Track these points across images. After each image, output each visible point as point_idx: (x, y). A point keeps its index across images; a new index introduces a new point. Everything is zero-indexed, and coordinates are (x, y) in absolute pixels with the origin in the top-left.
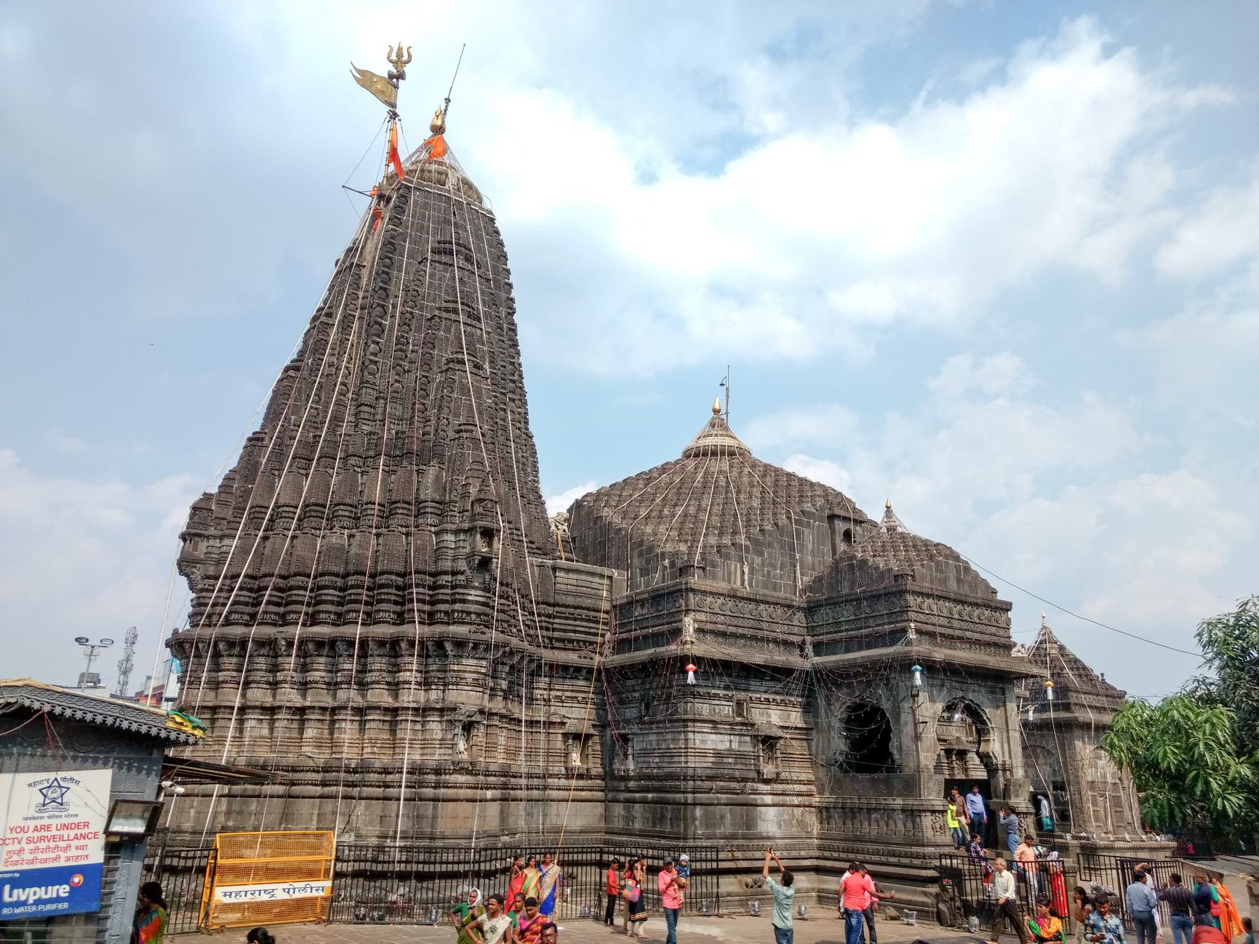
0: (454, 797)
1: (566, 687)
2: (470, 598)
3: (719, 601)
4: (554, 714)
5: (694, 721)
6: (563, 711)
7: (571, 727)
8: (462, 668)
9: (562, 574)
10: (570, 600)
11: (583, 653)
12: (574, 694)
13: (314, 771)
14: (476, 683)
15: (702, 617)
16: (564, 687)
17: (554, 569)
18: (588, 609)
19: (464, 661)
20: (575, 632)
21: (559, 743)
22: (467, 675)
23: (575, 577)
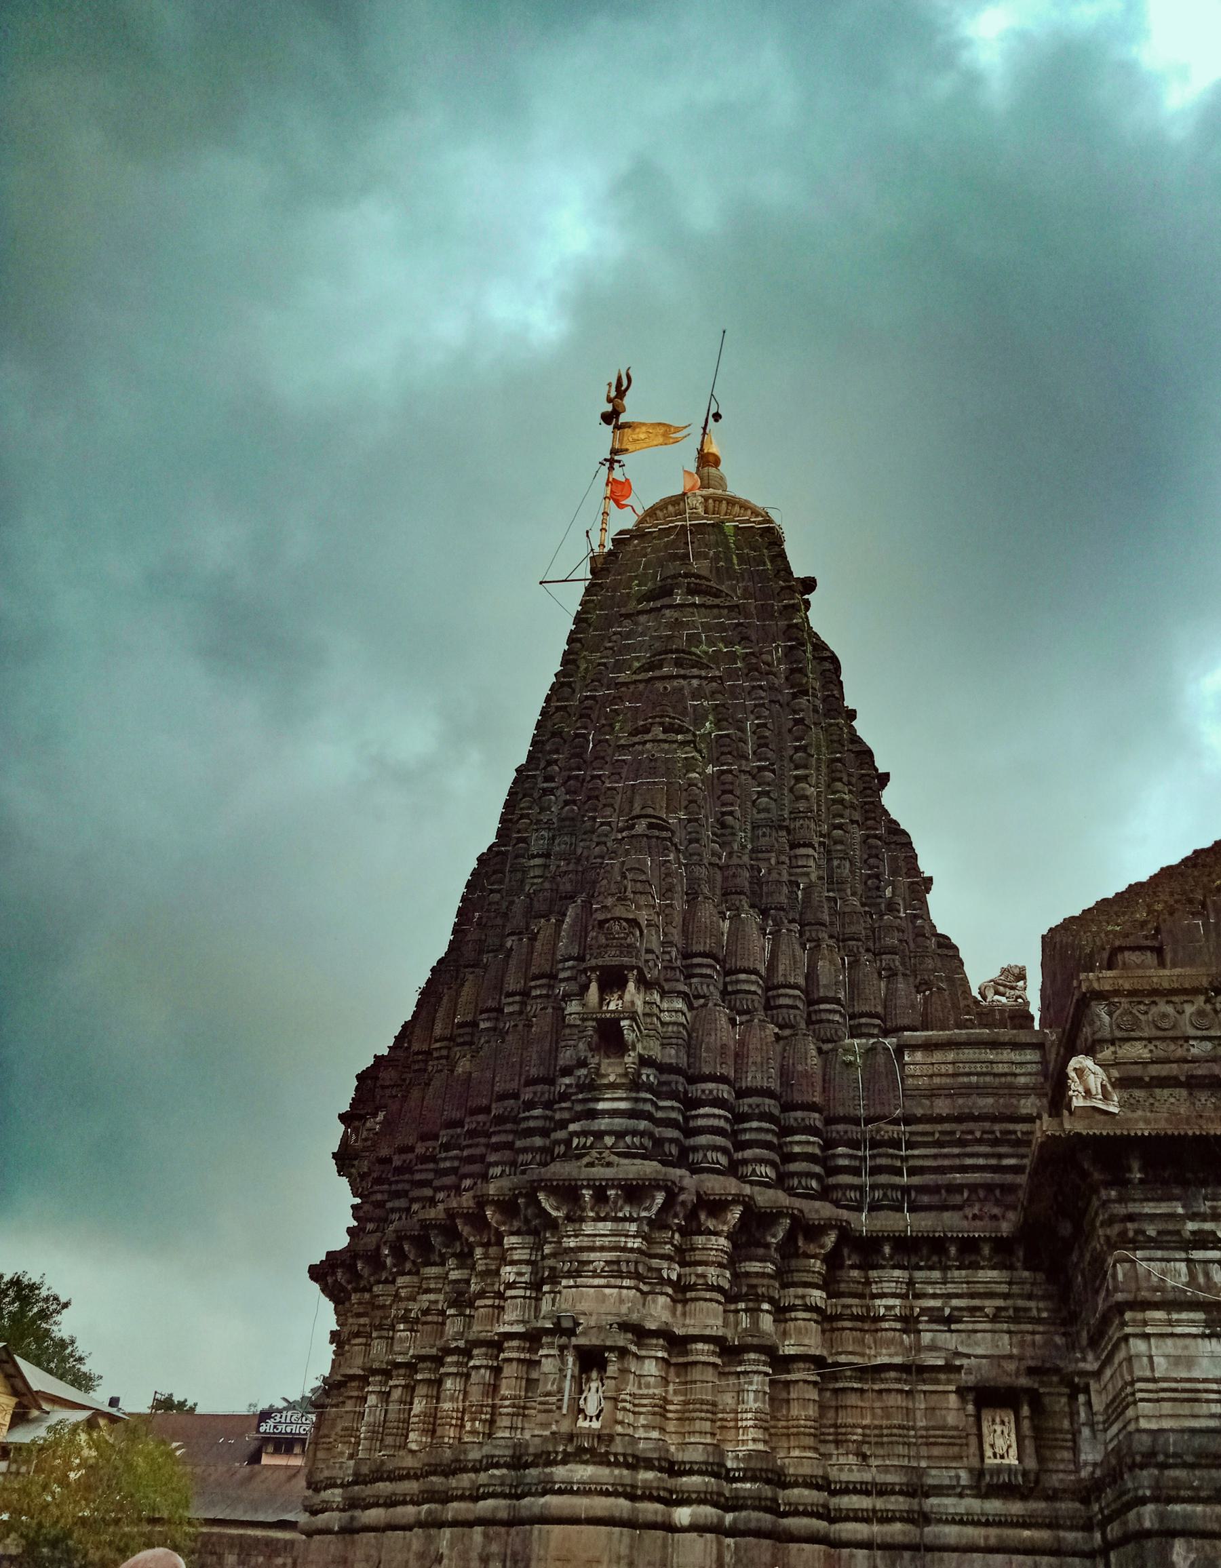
0: (566, 1513)
1: (951, 1288)
2: (601, 1106)
3: (1189, 1009)
4: (933, 1348)
5: (798, 1271)
6: (950, 1341)
7: (975, 1370)
8: (586, 1242)
9: (919, 1056)
10: (942, 1107)
11: (969, 1212)
12: (976, 1302)
13: (807, 1485)
14: (615, 1271)
15: (1138, 1051)
16: (938, 1286)
17: (900, 1050)
18: (994, 1119)
19: (588, 1228)
20: (964, 1169)
21: (953, 1411)
22: (592, 1256)
23: (951, 1056)
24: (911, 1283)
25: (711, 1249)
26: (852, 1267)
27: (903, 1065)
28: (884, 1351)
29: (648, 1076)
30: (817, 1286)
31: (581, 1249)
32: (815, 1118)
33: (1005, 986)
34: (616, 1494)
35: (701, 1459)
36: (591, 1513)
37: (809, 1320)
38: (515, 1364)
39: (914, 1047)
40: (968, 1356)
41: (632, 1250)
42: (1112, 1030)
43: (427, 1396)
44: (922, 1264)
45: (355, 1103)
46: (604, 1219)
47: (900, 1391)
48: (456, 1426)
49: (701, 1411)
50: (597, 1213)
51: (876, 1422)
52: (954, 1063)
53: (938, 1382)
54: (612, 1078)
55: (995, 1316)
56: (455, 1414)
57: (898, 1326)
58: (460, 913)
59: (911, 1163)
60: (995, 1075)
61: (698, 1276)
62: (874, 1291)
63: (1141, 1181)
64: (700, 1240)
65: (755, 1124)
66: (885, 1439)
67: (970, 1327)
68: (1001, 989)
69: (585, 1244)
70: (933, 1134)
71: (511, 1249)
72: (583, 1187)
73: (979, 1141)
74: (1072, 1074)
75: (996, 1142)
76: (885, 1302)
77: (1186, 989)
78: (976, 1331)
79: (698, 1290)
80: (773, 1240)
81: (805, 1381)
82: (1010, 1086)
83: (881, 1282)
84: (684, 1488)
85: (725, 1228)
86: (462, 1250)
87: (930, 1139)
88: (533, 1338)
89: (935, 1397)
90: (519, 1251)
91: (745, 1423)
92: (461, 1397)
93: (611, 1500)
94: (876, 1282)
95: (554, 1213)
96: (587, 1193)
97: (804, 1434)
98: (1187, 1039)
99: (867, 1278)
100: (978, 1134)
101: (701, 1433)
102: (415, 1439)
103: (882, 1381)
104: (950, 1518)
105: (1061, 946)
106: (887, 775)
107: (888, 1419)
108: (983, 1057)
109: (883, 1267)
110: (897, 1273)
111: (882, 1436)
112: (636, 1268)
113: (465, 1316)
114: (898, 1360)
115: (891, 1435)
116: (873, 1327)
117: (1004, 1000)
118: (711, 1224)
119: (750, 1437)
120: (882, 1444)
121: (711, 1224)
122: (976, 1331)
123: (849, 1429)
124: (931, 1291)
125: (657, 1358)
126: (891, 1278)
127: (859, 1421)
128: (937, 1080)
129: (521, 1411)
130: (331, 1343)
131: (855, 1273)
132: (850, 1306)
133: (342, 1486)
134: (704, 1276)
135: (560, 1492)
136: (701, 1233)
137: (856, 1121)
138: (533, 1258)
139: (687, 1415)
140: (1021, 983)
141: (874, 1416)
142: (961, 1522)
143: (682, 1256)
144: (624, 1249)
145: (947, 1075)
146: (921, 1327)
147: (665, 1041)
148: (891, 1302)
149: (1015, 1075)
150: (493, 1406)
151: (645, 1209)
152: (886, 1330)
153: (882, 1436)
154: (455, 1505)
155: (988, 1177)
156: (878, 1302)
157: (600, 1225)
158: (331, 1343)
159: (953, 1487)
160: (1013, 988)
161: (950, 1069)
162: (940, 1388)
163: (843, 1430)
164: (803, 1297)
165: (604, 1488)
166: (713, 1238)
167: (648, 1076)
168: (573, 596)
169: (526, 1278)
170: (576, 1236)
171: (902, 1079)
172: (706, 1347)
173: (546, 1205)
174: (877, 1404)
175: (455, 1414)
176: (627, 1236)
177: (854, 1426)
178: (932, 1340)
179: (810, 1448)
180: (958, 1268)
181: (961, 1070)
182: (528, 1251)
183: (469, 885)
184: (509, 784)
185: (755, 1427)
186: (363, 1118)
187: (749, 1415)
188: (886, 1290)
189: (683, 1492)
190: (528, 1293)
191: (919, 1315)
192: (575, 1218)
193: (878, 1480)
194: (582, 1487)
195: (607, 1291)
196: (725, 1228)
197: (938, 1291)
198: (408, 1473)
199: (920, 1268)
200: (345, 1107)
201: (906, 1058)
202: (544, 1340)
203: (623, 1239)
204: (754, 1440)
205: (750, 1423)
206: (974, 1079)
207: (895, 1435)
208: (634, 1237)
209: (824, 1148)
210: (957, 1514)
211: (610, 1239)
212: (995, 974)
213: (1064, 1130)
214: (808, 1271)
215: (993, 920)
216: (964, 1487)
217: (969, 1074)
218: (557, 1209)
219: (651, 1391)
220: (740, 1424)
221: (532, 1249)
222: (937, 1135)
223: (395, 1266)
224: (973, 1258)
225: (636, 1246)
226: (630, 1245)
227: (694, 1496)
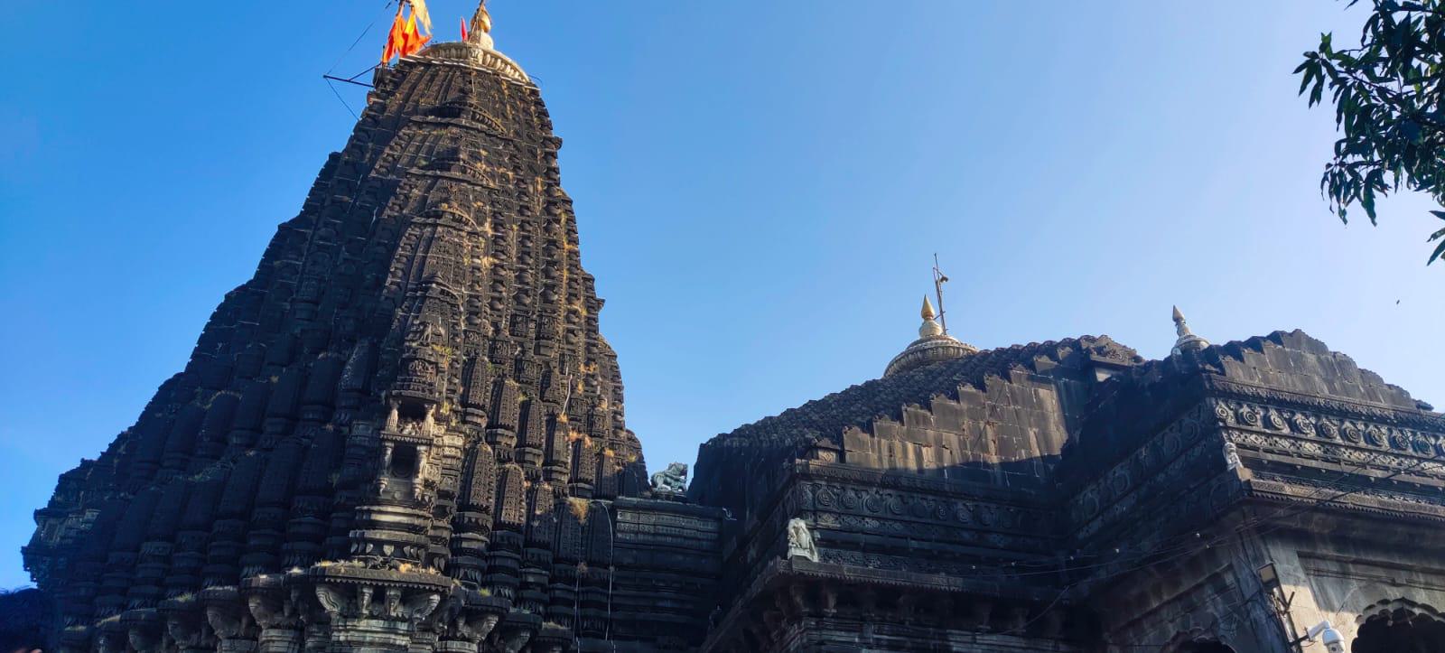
9: (628, 516)
19: (363, 624)
27: (615, 522)
32: (547, 555)
33: (672, 478)
39: (627, 508)
42: (814, 504)
50: (371, 612)
59: (616, 600)
63: (834, 616)
65: (504, 553)
68: (669, 479)
71: (268, 641)
74: (792, 531)
77: (864, 482)
86: (198, 643)
95: (328, 607)
96: (368, 593)
98: (864, 517)
105: (714, 454)
106: (603, 301)
117: (669, 488)
128: (641, 537)
136: (454, 638)
140: (683, 477)
145: (648, 533)
151: (419, 611)
157: (374, 622)
160: (677, 480)
161: (652, 529)
171: (614, 533)
173: (323, 600)
181: (661, 532)
184: (311, 183)
192: (351, 613)
200: (43, 504)
201: (619, 517)
206: (669, 539)
208: (403, 635)
209: (551, 582)
211: (379, 635)
212: (665, 468)
213: (792, 571)
217: (665, 535)
218: (333, 605)
221: (290, 642)
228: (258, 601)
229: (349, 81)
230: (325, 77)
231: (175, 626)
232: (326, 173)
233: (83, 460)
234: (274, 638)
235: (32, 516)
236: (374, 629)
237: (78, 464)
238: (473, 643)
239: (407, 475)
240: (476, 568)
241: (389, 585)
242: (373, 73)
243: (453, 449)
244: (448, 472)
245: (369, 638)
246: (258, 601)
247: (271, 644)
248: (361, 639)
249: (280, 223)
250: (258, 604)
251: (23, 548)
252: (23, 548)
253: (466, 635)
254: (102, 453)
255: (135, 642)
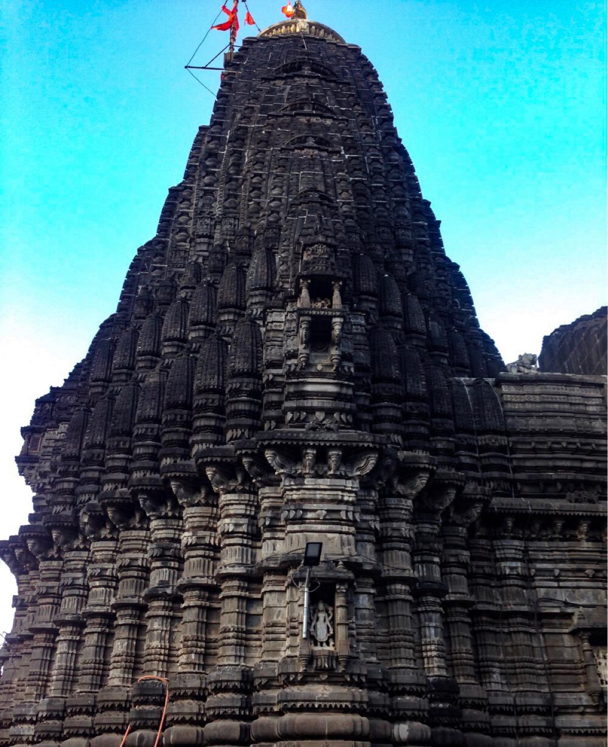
2: (309, 388)
8: (308, 495)
20: (555, 469)
23: (537, 389)
24: (526, 551)
25: (402, 509)
26: (481, 537)
28: (511, 602)
29: (349, 368)
30: (463, 548)
31: (303, 500)
34: (352, 711)
35: (414, 681)
36: (334, 729)
37: (461, 574)
38: (235, 601)
40: (577, 606)
41: (347, 503)
43: (128, 639)
44: (534, 536)
45: (35, 420)
46: (321, 477)
47: (526, 633)
48: (164, 661)
49: (405, 641)
51: (509, 658)
52: (539, 394)
53: (553, 626)
54: (319, 367)
55: (594, 576)
56: (163, 651)
57: (520, 583)
58: (126, 285)
60: (571, 404)
61: (394, 529)
62: (498, 556)
64: (393, 502)
66: (518, 670)
67: (575, 584)
69: (306, 497)
70: (530, 443)
71: (228, 505)
72: (309, 447)
73: (565, 450)
75: (577, 451)
76: (509, 564)
78: (578, 588)
79: (393, 541)
80: (441, 508)
81: (463, 622)
82: (586, 413)
83: (503, 549)
84: (400, 707)
85: (414, 492)
87: (528, 447)
88: (252, 579)
89: (552, 637)
90: (235, 507)
91: (429, 654)
92: (167, 636)
93: (349, 717)
94: (499, 549)
97: (467, 665)
99: (492, 546)
100: (564, 444)
101: (406, 659)
102: (115, 677)
103: (509, 625)
104: (577, 731)
107: (518, 654)
108: (561, 391)
109: (504, 538)
110: (516, 543)
111: (515, 668)
112: (354, 517)
113: (169, 568)
114: (525, 608)
115: (523, 667)
116: (499, 584)
118: (400, 488)
119: (436, 665)
120: (516, 674)
121: (400, 488)
122: (578, 588)
123: (490, 663)
124: (541, 557)
125: (369, 594)
126: (512, 546)
127: (496, 657)
129: (244, 639)
130: (13, 607)
131: (483, 542)
132: (482, 567)
133: (32, 722)
134: (398, 530)
135: (301, 710)
136: (392, 496)
137: (471, 432)
138: (248, 513)
139: (392, 644)
141: (506, 654)
142: (586, 734)
143: (380, 511)
144: (341, 502)
146: (537, 583)
147: (358, 347)
148: (514, 564)
149: (586, 405)
150: (207, 641)
152: (511, 585)
153: (515, 668)
154: (175, 728)
155: (571, 475)
156: (503, 564)
157: (320, 481)
158: (13, 607)
159: (577, 707)
162: (557, 631)
163: (485, 663)
164: (456, 556)
165: (344, 705)
166: (403, 500)
167: (349, 368)
168: (214, 81)
169: (244, 529)
170: (298, 490)
172: (404, 587)
174: (509, 643)
175: (163, 651)
176: (343, 491)
177: (493, 661)
178: (546, 593)
179: (472, 676)
180: (562, 540)
182: (244, 507)
183: (132, 267)
185: (438, 657)
186: (41, 431)
187: (433, 647)
188: (508, 556)
189: (399, 710)
190: (245, 541)
191: (535, 575)
193: (518, 703)
194: (323, 704)
195: (330, 535)
196: (414, 492)
197: (547, 557)
198: (113, 705)
199: (533, 540)
202: (266, 578)
203: (340, 493)
204: (439, 667)
205: (434, 653)
207: (527, 667)
210: (582, 728)
214: (458, 536)
215: (516, 321)
216: (586, 707)
219: (367, 622)
220: (425, 654)
222: (533, 444)
223: (92, 532)
224: (573, 532)
225: (351, 499)
226: (346, 498)
227: (409, 713)
228: (214, 469)
229: (203, 68)
230: (186, 67)
231: (145, 500)
232: (198, 141)
233: (52, 388)
234: (232, 502)
235: (20, 433)
236: (322, 487)
237: (48, 391)
238: (409, 499)
239: (325, 349)
240: (397, 432)
241: (331, 445)
242: (222, 57)
243: (359, 327)
244: (358, 347)
245: (319, 495)
246: (214, 469)
247: (230, 507)
248: (312, 496)
249: (170, 187)
250: (214, 471)
251: (16, 457)
252: (16, 457)
253: (401, 492)
254: (65, 380)
255: (113, 517)
